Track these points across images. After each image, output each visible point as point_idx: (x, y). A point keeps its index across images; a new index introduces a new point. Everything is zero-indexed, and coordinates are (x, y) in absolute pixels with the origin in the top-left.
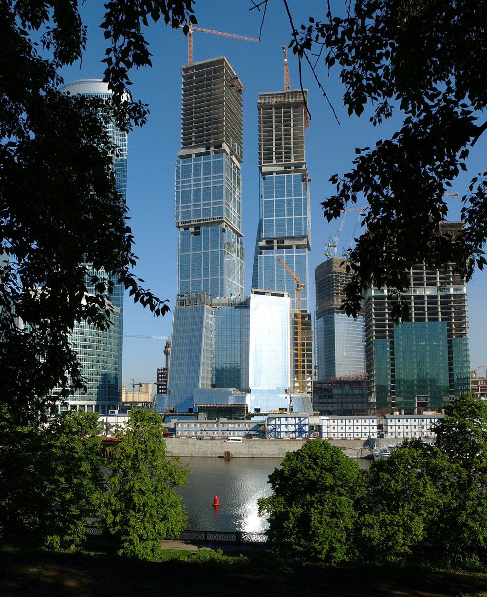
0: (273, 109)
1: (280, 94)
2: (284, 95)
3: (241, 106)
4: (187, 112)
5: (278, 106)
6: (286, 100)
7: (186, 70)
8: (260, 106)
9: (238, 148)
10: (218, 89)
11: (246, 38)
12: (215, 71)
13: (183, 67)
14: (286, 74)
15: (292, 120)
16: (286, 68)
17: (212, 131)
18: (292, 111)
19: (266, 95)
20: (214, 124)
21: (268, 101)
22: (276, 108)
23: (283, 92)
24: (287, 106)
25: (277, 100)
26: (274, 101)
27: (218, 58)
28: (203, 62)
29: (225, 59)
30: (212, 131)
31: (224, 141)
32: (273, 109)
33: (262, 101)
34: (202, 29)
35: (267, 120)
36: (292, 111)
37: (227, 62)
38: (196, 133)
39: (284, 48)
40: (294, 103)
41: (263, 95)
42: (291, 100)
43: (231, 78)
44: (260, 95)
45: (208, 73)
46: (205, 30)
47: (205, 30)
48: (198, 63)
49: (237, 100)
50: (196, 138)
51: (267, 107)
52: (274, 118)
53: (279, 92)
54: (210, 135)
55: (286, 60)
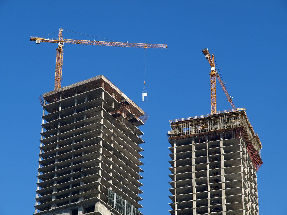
0: (193, 142)
1: (202, 119)
2: (209, 120)
3: (138, 143)
4: (47, 160)
5: (200, 138)
6: (213, 128)
7: (49, 99)
8: (173, 139)
9: (128, 207)
10: (93, 122)
11: (146, 45)
12: (90, 97)
13: (45, 95)
14: (214, 87)
15: (222, 158)
16: (215, 79)
17: (82, 185)
18: (222, 144)
19: (180, 123)
20: (85, 175)
21: (185, 130)
22: (197, 141)
23: (206, 116)
24: (214, 136)
25: (199, 128)
26: (193, 131)
27: (93, 79)
28: (72, 86)
29: (103, 78)
30: (82, 185)
31: (97, 200)
32: (193, 142)
33: (176, 132)
34: (78, 41)
35: (183, 161)
36: (222, 144)
37: (107, 81)
38: (58, 190)
39: (206, 53)
40: (224, 131)
41: (176, 123)
42: (221, 127)
43: (116, 104)
44: (172, 124)
45: (80, 100)
46: (81, 41)
47: (81, 41)
48: (65, 88)
49: (131, 136)
50: (58, 197)
51: (182, 141)
52: (194, 155)
53: (201, 117)
54: (77, 192)
55: (213, 69)
